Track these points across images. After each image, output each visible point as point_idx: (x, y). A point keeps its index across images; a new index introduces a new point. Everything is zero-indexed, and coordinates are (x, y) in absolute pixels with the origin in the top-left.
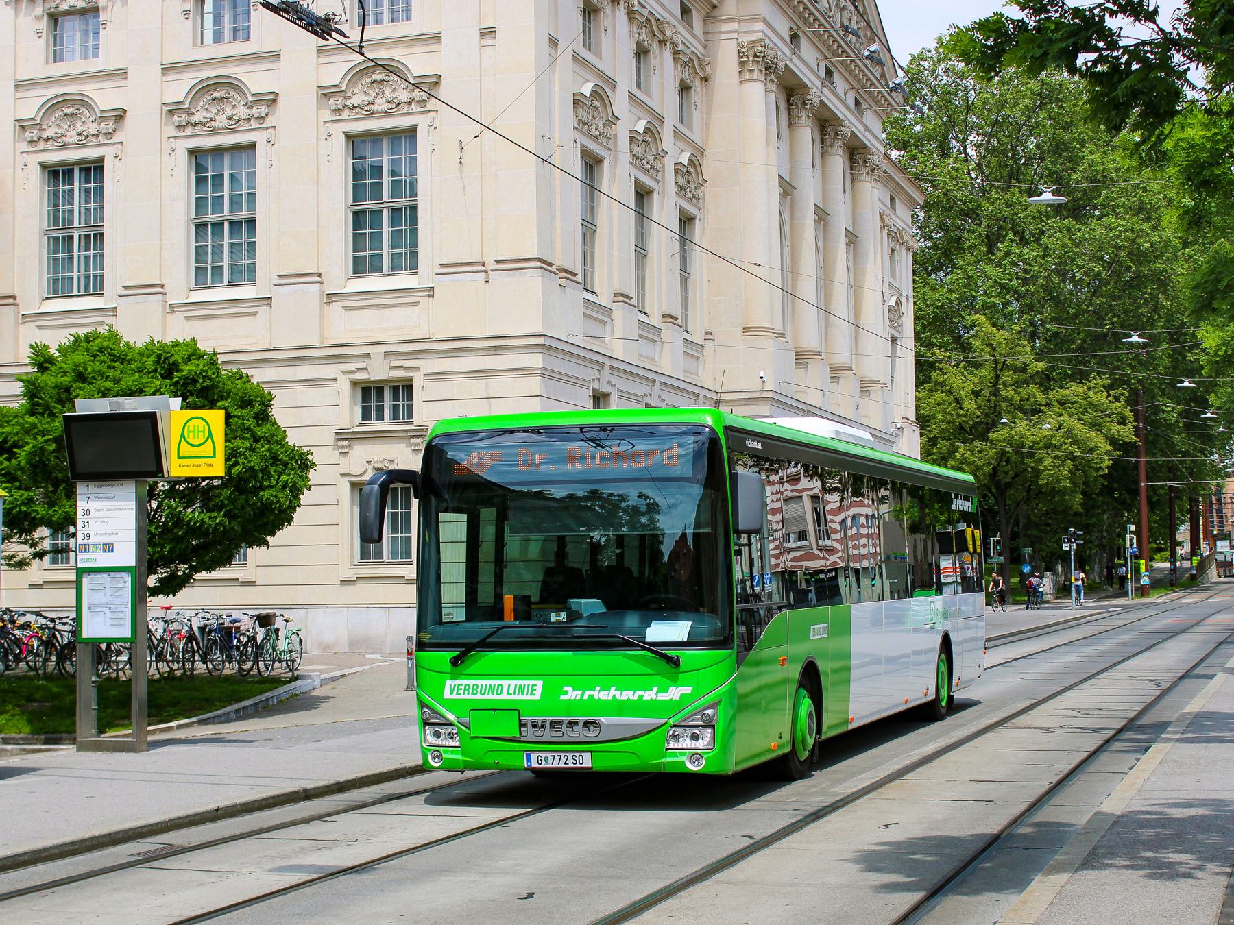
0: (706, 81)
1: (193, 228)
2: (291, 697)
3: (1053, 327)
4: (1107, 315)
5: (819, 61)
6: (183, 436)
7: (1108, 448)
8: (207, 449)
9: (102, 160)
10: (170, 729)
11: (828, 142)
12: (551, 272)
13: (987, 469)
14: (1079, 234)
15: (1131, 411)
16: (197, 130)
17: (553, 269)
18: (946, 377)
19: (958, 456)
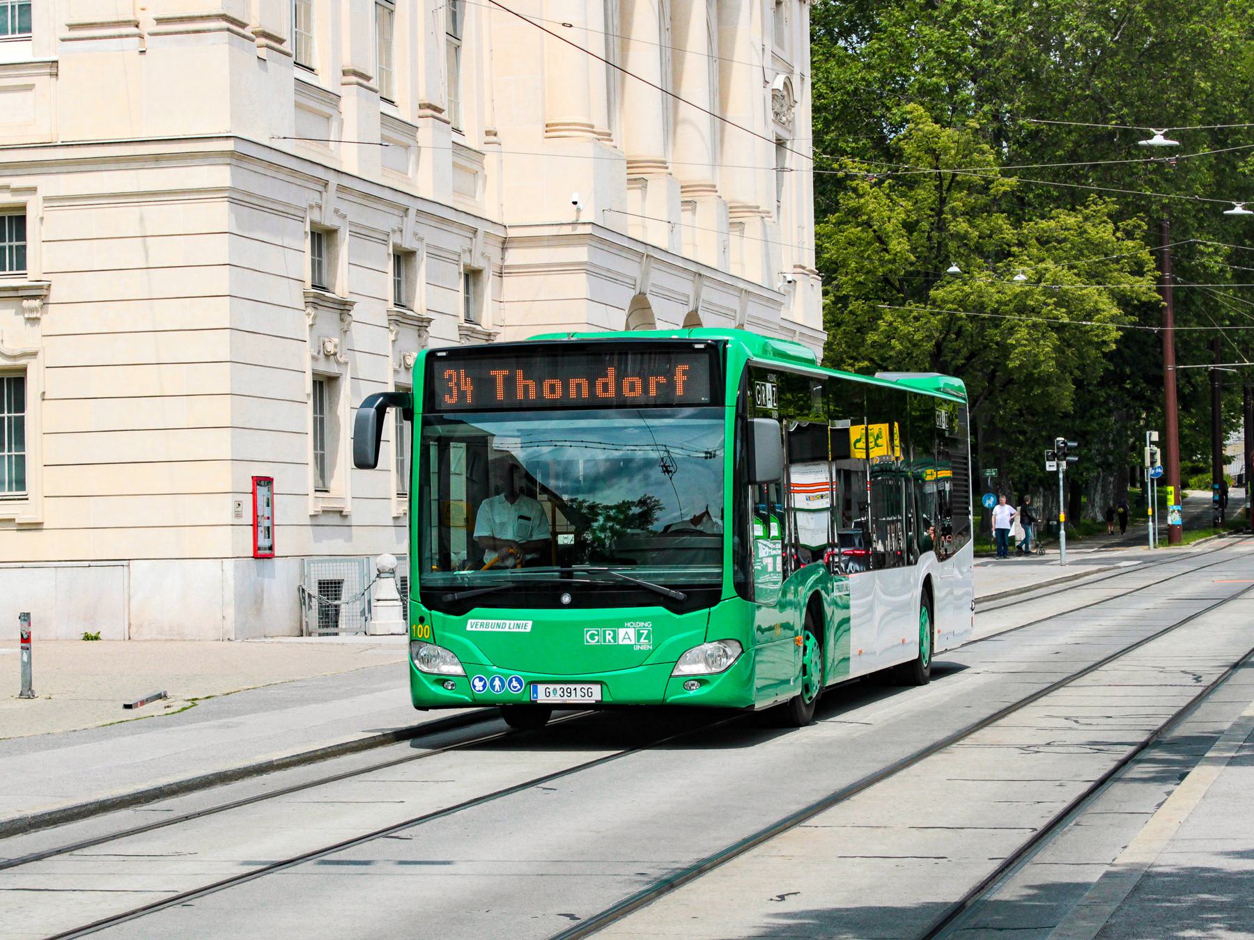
3: (1028, 123)
7: (1116, 311)
12: (244, 37)
13: (929, 346)
15: (1152, 253)
17: (247, 32)
18: (862, 201)
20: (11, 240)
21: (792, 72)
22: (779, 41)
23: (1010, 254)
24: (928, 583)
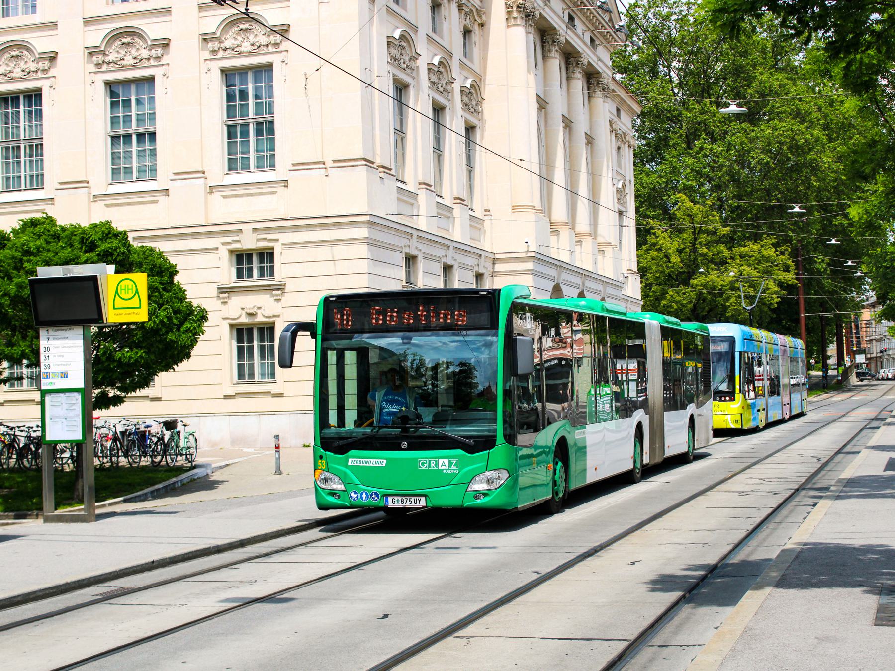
0: (482, 26)
1: (109, 139)
2: (191, 481)
5: (564, 10)
6: (117, 292)
7: (777, 289)
8: (135, 302)
9: (40, 90)
10: (104, 506)
11: (571, 69)
12: (373, 168)
13: (690, 306)
14: (753, 134)
15: (793, 262)
16: (112, 67)
17: (375, 166)
23: (727, 263)
24: (692, 418)
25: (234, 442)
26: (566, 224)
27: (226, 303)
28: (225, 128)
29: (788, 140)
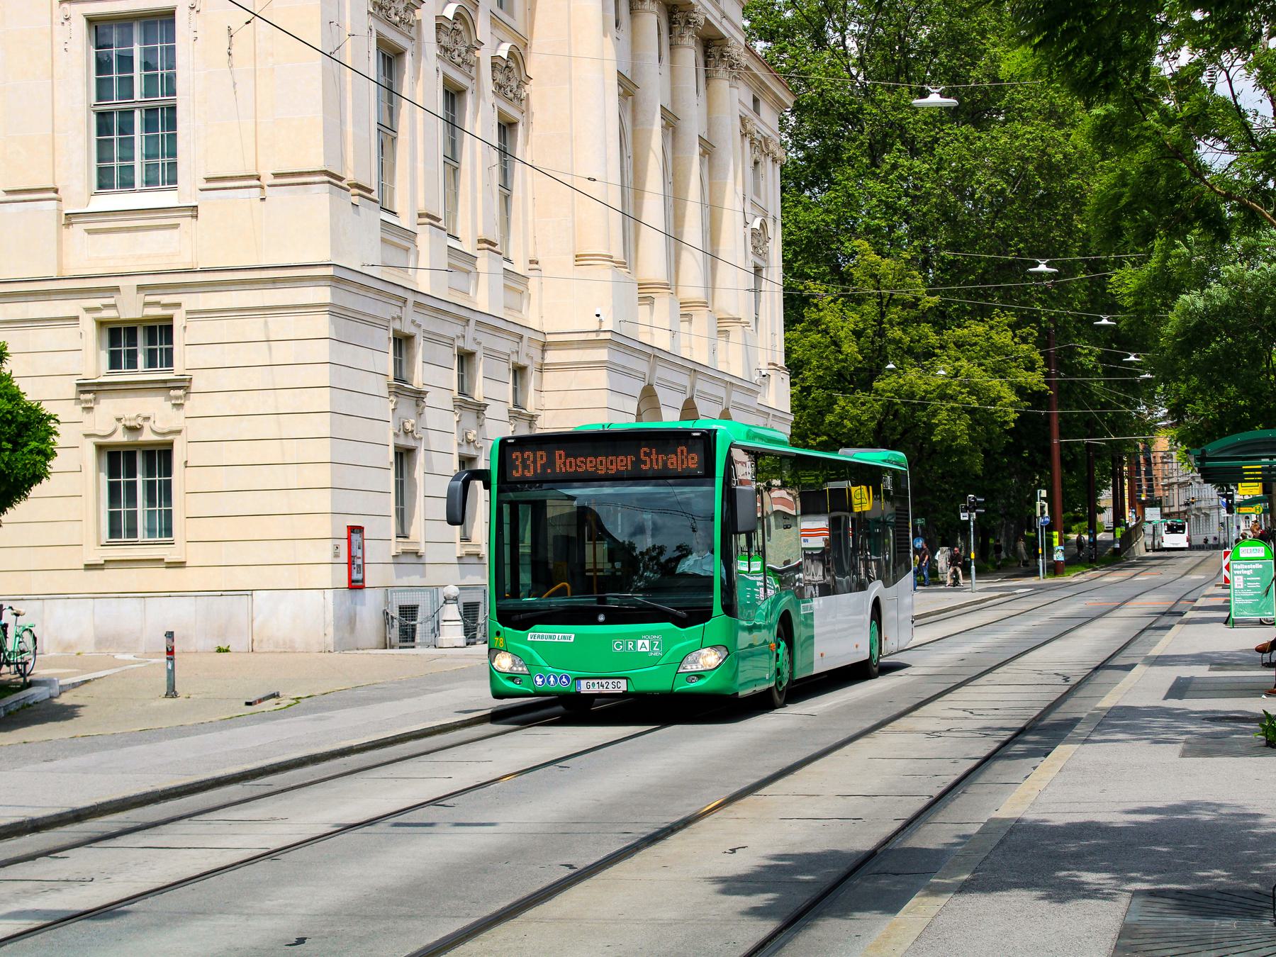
2: (23, 707)
3: (947, 254)
4: (1012, 239)
7: (1014, 398)
11: (677, 32)
13: (873, 425)
14: (979, 144)
15: (1041, 354)
17: (344, 184)
18: (822, 314)
19: (837, 409)
20: (161, 344)
21: (766, 216)
22: (757, 192)
23: (934, 355)
24: (876, 604)
25: (102, 641)
26: (666, 286)
27: (91, 409)
28: (94, 117)
29: (1035, 155)
